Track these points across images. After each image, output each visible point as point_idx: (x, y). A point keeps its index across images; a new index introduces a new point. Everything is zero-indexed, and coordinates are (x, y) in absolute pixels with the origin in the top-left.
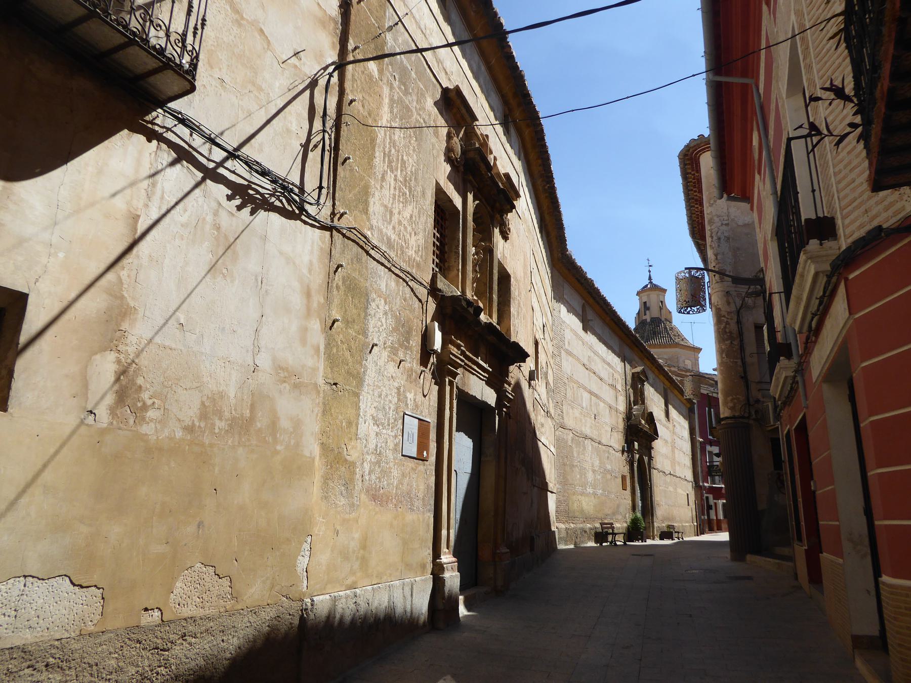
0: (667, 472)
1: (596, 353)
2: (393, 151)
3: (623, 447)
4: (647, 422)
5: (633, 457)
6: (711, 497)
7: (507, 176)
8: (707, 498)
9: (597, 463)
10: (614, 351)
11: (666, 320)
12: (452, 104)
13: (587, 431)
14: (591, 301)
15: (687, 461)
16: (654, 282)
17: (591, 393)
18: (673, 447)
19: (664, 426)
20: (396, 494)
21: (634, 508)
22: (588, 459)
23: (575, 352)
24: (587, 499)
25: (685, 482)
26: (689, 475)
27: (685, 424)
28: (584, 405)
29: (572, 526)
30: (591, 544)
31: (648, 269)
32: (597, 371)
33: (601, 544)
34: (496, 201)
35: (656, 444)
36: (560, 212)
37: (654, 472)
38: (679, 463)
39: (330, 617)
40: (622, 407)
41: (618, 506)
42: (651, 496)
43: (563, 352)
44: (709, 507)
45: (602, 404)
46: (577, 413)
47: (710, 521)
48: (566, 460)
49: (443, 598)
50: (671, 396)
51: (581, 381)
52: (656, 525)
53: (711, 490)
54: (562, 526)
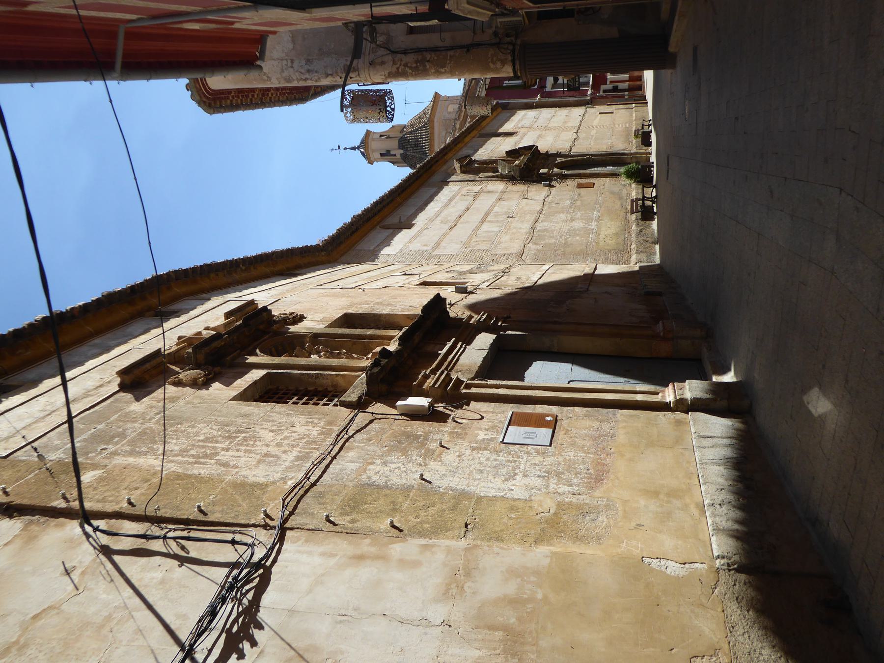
0: (575, 136)
1: (437, 215)
2: (192, 452)
3: (545, 185)
4: (517, 158)
5: (556, 175)
6: (603, 87)
7: (228, 315)
8: (605, 91)
9: (563, 216)
11: (401, 131)
12: (138, 380)
13: (526, 226)
14: (377, 218)
15: (563, 113)
16: (357, 144)
17: (483, 221)
18: (547, 128)
19: (522, 138)
20: (595, 454)
21: (614, 175)
22: (558, 226)
23: (436, 239)
24: (603, 229)
25: (586, 115)
26: (578, 111)
27: (521, 114)
28: (497, 229)
29: (634, 246)
31: (342, 151)
32: (457, 214)
33: (655, 214)
34: (257, 330)
35: (543, 147)
36: (274, 253)
37: (575, 151)
38: (565, 122)
41: (612, 193)
42: (601, 155)
43: (436, 253)
44: (615, 89)
45: (496, 209)
46: (505, 238)
47: (630, 89)
48: (559, 252)
49: (714, 400)
50: (488, 130)
51: (469, 232)
54: (634, 258)
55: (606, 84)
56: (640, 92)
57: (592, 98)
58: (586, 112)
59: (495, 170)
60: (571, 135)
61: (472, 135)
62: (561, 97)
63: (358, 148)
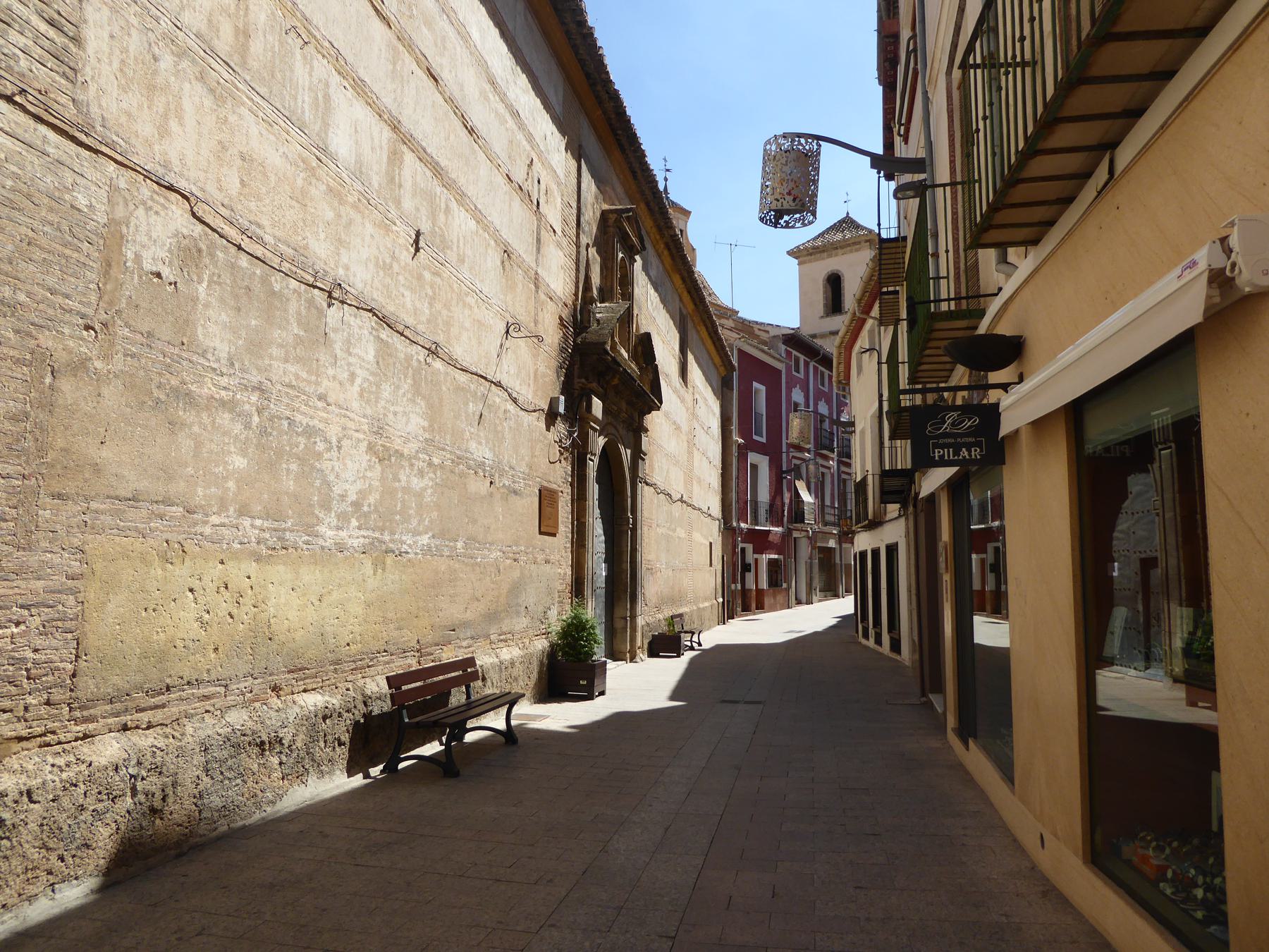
0: (676, 496)
3: (553, 403)
4: (634, 357)
5: (584, 437)
6: (749, 548)
8: (743, 550)
10: (547, 106)
15: (713, 478)
18: (691, 444)
19: (675, 391)
21: (578, 588)
25: (708, 520)
26: (714, 504)
27: (715, 406)
30: (341, 782)
35: (654, 420)
37: (645, 493)
38: (699, 481)
39: (192, 822)
40: (559, 278)
41: (516, 589)
42: (634, 550)
44: (746, 568)
47: (745, 592)
50: (692, 336)
52: (640, 621)
55: (755, 552)
56: (739, 609)
57: (734, 529)
59: (605, 295)
60: (677, 489)
62: (738, 478)
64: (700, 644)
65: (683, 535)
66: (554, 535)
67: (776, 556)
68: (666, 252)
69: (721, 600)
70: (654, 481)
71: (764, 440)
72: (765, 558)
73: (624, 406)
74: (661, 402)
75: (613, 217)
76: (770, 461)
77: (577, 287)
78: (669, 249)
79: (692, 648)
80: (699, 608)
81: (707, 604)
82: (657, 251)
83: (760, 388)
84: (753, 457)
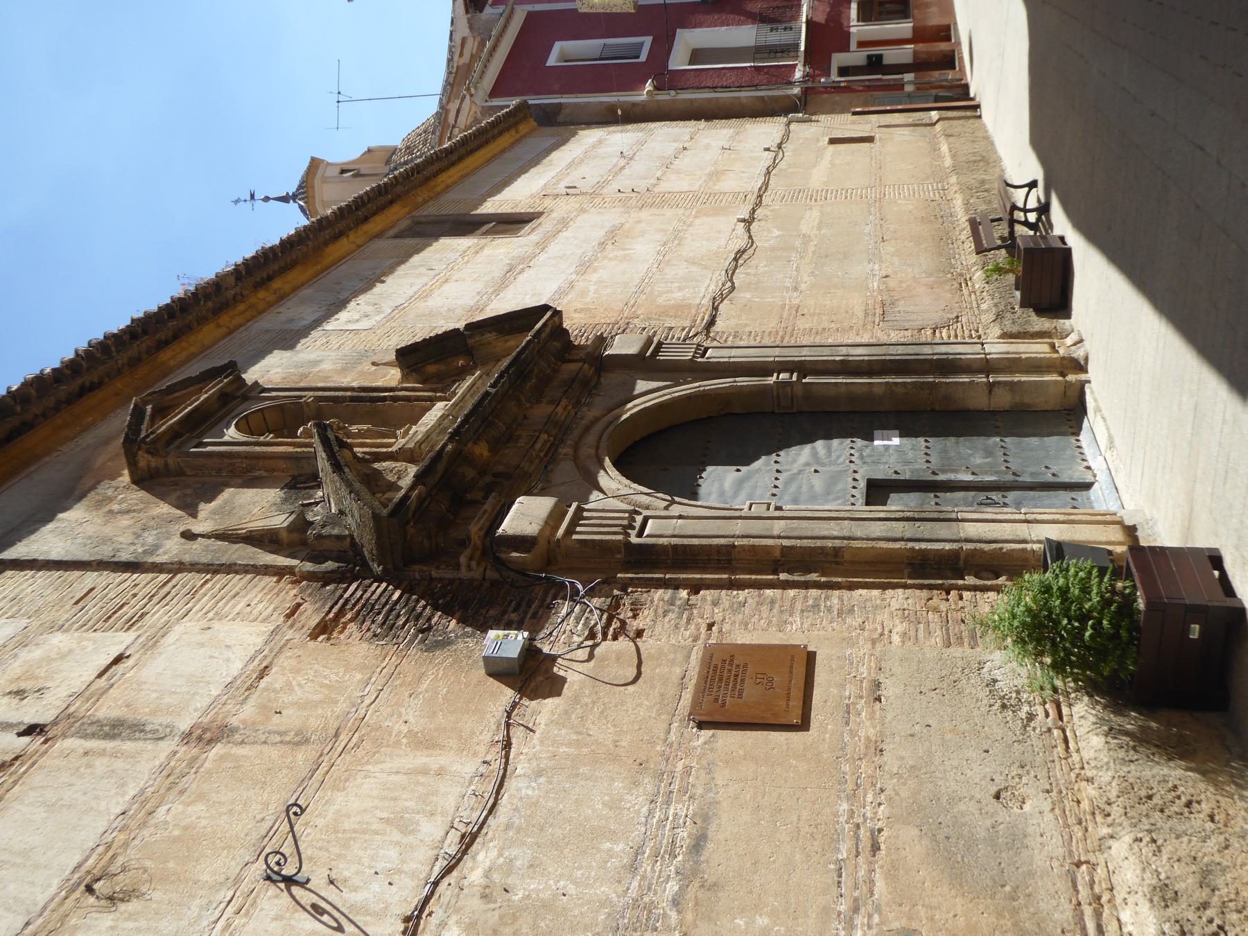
0: (741, 243)
3: (499, 671)
6: (839, 59)
8: (843, 71)
11: (388, 162)
16: (292, 189)
25: (788, 148)
26: (763, 133)
27: (589, 137)
31: (259, 204)
38: (716, 175)
42: (846, 368)
44: (875, 64)
47: (919, 65)
50: (448, 205)
52: (996, 348)
53: (818, 54)
55: (846, 48)
56: (950, 75)
57: (806, 92)
58: (786, 136)
60: (721, 234)
61: (373, 226)
63: (294, 197)
64: (1033, 185)
65: (813, 216)
66: (811, 657)
67: (854, 6)
68: (276, 284)
69: (934, 115)
70: (707, 302)
71: (648, 41)
72: (857, 28)
73: (541, 411)
74: (545, 308)
75: (144, 460)
76: (683, 26)
77: (265, 570)
78: (270, 278)
79: (1044, 209)
80: (955, 169)
81: (944, 148)
82: (270, 305)
83: (559, 52)
84: (678, 61)
